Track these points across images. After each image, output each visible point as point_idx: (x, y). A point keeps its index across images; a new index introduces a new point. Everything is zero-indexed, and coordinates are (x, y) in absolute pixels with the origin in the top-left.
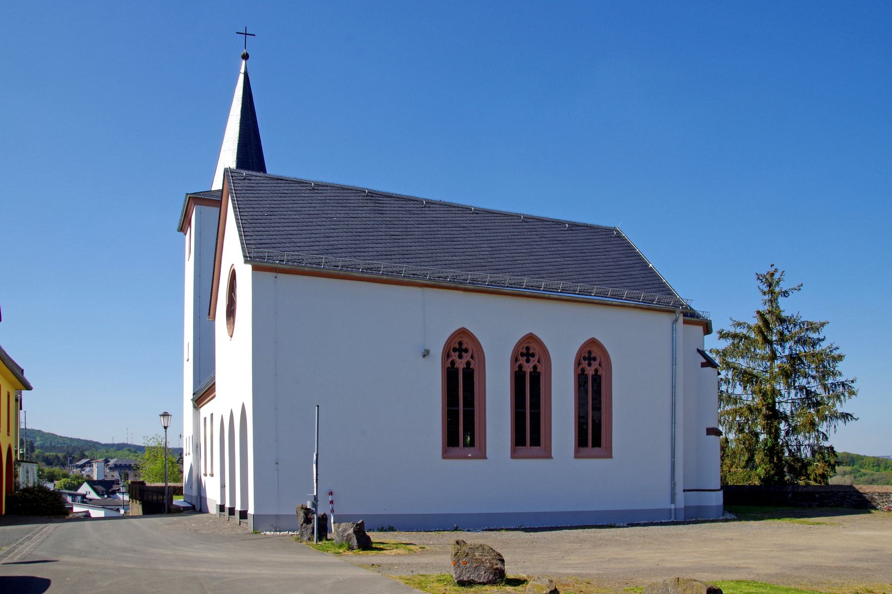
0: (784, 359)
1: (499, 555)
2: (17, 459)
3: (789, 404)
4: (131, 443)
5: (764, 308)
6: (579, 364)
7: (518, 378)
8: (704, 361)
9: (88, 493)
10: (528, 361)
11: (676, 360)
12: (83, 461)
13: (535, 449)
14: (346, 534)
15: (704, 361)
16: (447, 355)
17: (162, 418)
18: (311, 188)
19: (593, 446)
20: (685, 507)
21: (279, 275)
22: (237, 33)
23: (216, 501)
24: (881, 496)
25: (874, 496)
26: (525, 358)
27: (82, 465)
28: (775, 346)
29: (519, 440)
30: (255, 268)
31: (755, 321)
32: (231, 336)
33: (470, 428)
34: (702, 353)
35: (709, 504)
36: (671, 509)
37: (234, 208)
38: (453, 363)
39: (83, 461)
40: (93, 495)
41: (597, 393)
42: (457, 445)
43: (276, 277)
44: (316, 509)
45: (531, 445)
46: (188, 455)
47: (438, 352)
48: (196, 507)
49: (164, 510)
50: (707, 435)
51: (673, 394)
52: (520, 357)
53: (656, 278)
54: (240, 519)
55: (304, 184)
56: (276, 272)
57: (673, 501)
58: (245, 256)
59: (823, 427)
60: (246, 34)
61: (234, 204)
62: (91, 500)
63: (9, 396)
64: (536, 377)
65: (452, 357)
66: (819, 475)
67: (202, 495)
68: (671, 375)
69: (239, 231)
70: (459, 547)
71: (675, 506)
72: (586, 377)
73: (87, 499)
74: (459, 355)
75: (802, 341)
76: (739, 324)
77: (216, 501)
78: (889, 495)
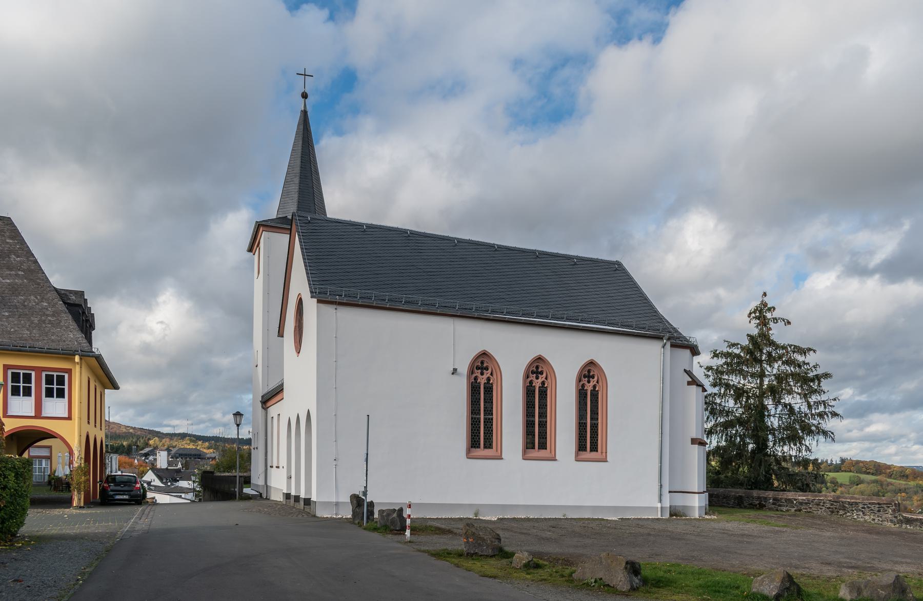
0: (773, 378)
1: (498, 535)
3: (777, 419)
4: (191, 433)
5: (755, 332)
9: (153, 481)
11: (664, 379)
12: (147, 450)
14: (391, 518)
16: (471, 371)
17: (235, 416)
19: (591, 451)
21: (338, 307)
22: (297, 74)
23: (283, 490)
24: (852, 505)
25: (845, 505)
26: (535, 375)
27: (145, 453)
28: (765, 365)
29: (529, 445)
30: (319, 301)
31: (745, 342)
32: (299, 353)
34: (689, 373)
36: (657, 508)
37: (300, 242)
39: (147, 450)
40: (157, 482)
43: (336, 309)
44: (366, 497)
46: (256, 449)
47: (464, 369)
49: (236, 498)
50: (692, 444)
52: (531, 375)
53: (651, 308)
54: (304, 505)
55: (357, 227)
56: (336, 304)
58: (311, 292)
59: (808, 441)
60: (305, 75)
61: (300, 239)
62: (155, 486)
63: (96, 389)
67: (268, 484)
68: (664, 391)
69: (306, 269)
70: (468, 528)
73: (151, 486)
74: (481, 372)
75: (790, 362)
76: (734, 345)
77: (283, 490)
78: (858, 504)
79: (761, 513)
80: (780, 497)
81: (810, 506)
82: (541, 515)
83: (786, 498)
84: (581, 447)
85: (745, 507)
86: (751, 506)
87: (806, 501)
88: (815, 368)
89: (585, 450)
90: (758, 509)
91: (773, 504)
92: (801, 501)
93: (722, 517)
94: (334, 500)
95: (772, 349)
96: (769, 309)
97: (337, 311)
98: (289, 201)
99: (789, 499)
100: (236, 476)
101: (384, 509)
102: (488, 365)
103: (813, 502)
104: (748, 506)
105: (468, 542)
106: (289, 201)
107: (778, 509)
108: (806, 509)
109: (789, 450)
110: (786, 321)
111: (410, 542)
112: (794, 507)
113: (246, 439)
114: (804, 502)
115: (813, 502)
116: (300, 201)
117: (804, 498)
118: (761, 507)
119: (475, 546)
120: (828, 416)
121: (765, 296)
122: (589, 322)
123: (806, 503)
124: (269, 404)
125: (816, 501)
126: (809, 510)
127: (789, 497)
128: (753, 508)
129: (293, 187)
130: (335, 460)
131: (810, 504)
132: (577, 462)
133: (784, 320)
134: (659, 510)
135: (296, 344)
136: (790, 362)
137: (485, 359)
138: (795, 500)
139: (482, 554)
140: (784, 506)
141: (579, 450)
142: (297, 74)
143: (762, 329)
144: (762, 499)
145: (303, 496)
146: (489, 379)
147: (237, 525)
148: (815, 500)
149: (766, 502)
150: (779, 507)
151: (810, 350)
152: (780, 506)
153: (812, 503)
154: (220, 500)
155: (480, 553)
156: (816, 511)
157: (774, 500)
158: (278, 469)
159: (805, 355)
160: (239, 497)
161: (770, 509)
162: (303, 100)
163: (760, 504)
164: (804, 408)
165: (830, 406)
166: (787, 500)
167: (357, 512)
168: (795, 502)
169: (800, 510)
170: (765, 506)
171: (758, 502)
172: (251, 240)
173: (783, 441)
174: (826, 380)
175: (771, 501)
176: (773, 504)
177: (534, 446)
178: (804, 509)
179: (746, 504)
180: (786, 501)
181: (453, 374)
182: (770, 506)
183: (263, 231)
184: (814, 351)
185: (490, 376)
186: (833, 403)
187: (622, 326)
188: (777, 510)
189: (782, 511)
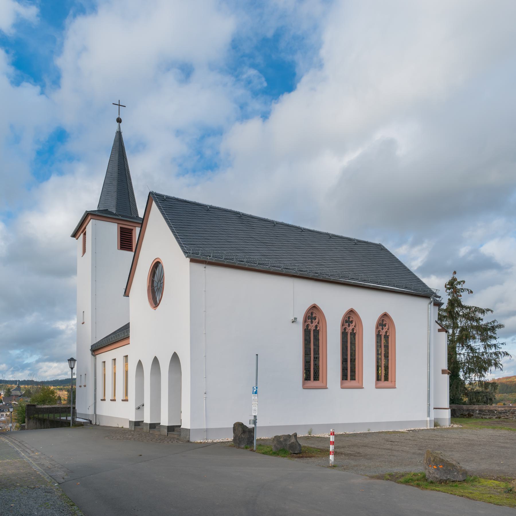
2: (11, 389)
6: (343, 325)
7: (344, 334)
8: (440, 328)
10: (349, 326)
11: (431, 327)
13: (386, 383)
15: (440, 328)
16: (305, 321)
18: (207, 209)
20: (434, 418)
22: (113, 104)
23: (129, 419)
26: (347, 324)
30: (192, 261)
33: (353, 371)
35: (446, 418)
36: (427, 420)
38: (345, 329)
41: (317, 339)
42: (310, 380)
43: (205, 267)
45: (351, 380)
47: (301, 319)
48: (92, 422)
50: (442, 374)
51: (429, 348)
54: (168, 431)
57: (429, 415)
60: (119, 105)
64: (317, 332)
65: (307, 322)
66: (489, 398)
71: (430, 419)
72: (347, 333)
77: (129, 419)
79: (472, 421)
80: (484, 409)
81: (507, 414)
82: (354, 431)
83: (489, 410)
84: (344, 377)
85: (458, 417)
86: (462, 416)
87: (504, 411)
88: (493, 322)
89: (310, 380)
90: (467, 417)
91: (479, 414)
92: (500, 411)
93: (465, 426)
94: (204, 427)
95: (460, 309)
96: (459, 283)
97: (206, 269)
98: (109, 198)
99: (491, 410)
100: (70, 408)
101: (279, 435)
102: (316, 315)
103: (509, 412)
104: (460, 416)
105: (438, 469)
106: (109, 198)
107: (483, 417)
108: (504, 416)
109: (474, 377)
110: (469, 291)
111: (334, 466)
112: (495, 416)
113: (22, 381)
114: (503, 412)
115: (509, 412)
116: (118, 198)
117: (503, 409)
118: (470, 416)
119: (445, 473)
120: (501, 355)
121: (455, 274)
122: (383, 284)
123: (504, 413)
124: (96, 353)
125: (511, 411)
126: (506, 417)
127: (491, 409)
128: (464, 417)
129: (112, 188)
130: (205, 393)
131: (507, 413)
132: (304, 389)
133: (468, 290)
134: (428, 422)
135: (150, 301)
136: (472, 319)
137: (315, 311)
138: (496, 410)
139: (454, 480)
140: (488, 415)
141: (343, 380)
142: (113, 104)
143: (453, 296)
144: (470, 411)
145: (165, 422)
146: (316, 327)
147: (141, 455)
148: (510, 410)
149: (474, 413)
150: (483, 416)
151: (488, 310)
152: (484, 415)
153: (508, 413)
154: (54, 428)
155: (452, 479)
156: (511, 417)
157: (479, 411)
158: (104, 402)
159: (484, 313)
160: (73, 425)
161: (477, 418)
162: (117, 124)
163: (469, 414)
164: (482, 350)
165: (499, 348)
166: (489, 411)
167: (242, 438)
168: (496, 412)
169: (500, 418)
170: (473, 416)
171: (467, 413)
172: (77, 227)
173: (470, 371)
174: (500, 329)
175: (477, 412)
176: (479, 414)
177: (347, 377)
178: (502, 416)
179: (458, 415)
180: (489, 412)
181: (293, 322)
182: (476, 416)
183: (91, 219)
184: (492, 311)
185: (318, 324)
186: (501, 346)
187: (406, 288)
188: (482, 418)
189: (486, 418)
